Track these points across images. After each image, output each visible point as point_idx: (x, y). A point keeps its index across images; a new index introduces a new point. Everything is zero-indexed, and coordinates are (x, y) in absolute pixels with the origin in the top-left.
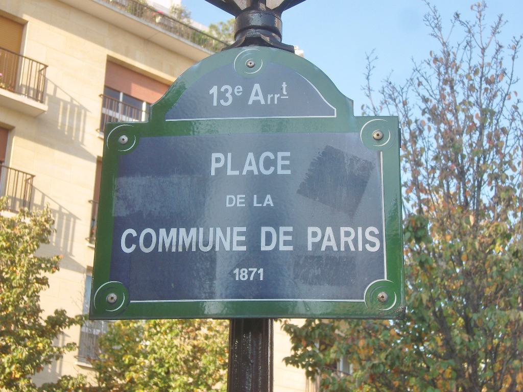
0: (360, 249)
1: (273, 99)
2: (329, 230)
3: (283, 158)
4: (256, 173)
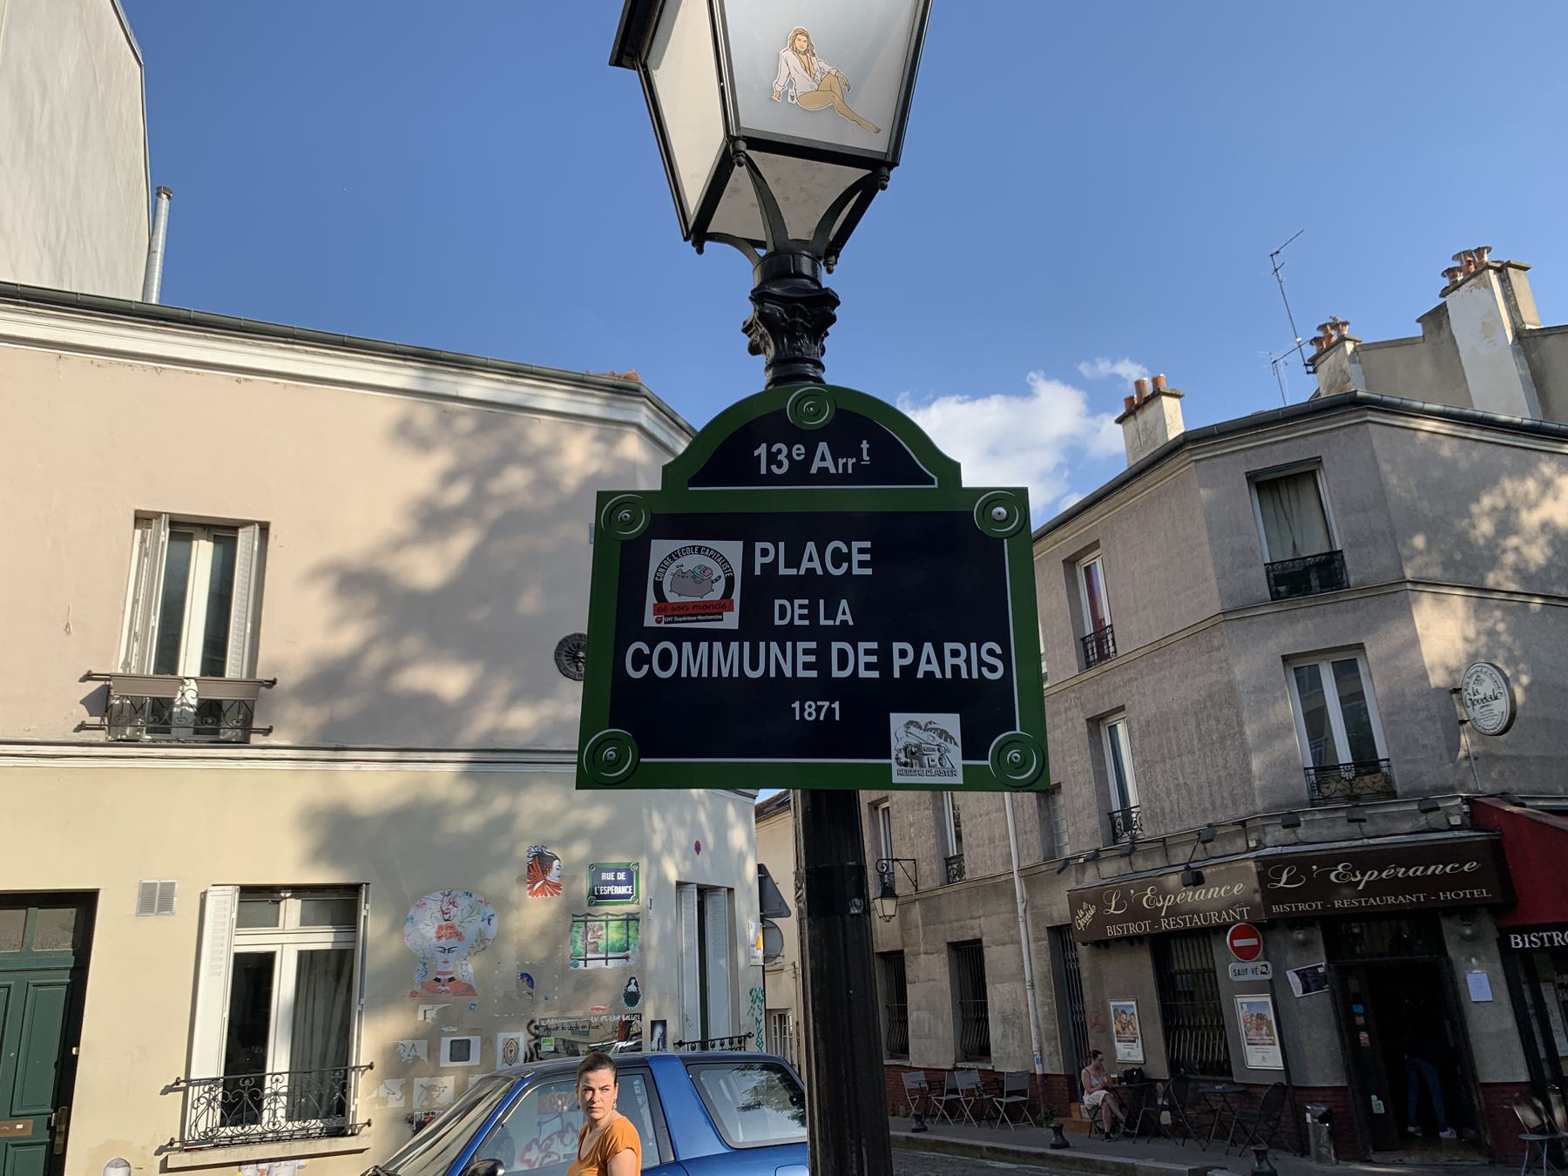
0: (975, 675)
1: (845, 465)
2: (928, 648)
3: (861, 551)
4: (820, 572)
